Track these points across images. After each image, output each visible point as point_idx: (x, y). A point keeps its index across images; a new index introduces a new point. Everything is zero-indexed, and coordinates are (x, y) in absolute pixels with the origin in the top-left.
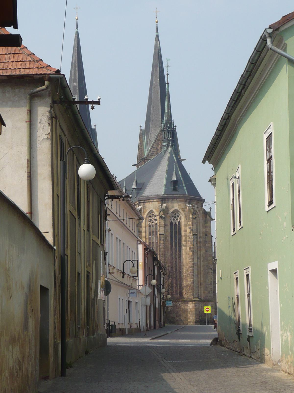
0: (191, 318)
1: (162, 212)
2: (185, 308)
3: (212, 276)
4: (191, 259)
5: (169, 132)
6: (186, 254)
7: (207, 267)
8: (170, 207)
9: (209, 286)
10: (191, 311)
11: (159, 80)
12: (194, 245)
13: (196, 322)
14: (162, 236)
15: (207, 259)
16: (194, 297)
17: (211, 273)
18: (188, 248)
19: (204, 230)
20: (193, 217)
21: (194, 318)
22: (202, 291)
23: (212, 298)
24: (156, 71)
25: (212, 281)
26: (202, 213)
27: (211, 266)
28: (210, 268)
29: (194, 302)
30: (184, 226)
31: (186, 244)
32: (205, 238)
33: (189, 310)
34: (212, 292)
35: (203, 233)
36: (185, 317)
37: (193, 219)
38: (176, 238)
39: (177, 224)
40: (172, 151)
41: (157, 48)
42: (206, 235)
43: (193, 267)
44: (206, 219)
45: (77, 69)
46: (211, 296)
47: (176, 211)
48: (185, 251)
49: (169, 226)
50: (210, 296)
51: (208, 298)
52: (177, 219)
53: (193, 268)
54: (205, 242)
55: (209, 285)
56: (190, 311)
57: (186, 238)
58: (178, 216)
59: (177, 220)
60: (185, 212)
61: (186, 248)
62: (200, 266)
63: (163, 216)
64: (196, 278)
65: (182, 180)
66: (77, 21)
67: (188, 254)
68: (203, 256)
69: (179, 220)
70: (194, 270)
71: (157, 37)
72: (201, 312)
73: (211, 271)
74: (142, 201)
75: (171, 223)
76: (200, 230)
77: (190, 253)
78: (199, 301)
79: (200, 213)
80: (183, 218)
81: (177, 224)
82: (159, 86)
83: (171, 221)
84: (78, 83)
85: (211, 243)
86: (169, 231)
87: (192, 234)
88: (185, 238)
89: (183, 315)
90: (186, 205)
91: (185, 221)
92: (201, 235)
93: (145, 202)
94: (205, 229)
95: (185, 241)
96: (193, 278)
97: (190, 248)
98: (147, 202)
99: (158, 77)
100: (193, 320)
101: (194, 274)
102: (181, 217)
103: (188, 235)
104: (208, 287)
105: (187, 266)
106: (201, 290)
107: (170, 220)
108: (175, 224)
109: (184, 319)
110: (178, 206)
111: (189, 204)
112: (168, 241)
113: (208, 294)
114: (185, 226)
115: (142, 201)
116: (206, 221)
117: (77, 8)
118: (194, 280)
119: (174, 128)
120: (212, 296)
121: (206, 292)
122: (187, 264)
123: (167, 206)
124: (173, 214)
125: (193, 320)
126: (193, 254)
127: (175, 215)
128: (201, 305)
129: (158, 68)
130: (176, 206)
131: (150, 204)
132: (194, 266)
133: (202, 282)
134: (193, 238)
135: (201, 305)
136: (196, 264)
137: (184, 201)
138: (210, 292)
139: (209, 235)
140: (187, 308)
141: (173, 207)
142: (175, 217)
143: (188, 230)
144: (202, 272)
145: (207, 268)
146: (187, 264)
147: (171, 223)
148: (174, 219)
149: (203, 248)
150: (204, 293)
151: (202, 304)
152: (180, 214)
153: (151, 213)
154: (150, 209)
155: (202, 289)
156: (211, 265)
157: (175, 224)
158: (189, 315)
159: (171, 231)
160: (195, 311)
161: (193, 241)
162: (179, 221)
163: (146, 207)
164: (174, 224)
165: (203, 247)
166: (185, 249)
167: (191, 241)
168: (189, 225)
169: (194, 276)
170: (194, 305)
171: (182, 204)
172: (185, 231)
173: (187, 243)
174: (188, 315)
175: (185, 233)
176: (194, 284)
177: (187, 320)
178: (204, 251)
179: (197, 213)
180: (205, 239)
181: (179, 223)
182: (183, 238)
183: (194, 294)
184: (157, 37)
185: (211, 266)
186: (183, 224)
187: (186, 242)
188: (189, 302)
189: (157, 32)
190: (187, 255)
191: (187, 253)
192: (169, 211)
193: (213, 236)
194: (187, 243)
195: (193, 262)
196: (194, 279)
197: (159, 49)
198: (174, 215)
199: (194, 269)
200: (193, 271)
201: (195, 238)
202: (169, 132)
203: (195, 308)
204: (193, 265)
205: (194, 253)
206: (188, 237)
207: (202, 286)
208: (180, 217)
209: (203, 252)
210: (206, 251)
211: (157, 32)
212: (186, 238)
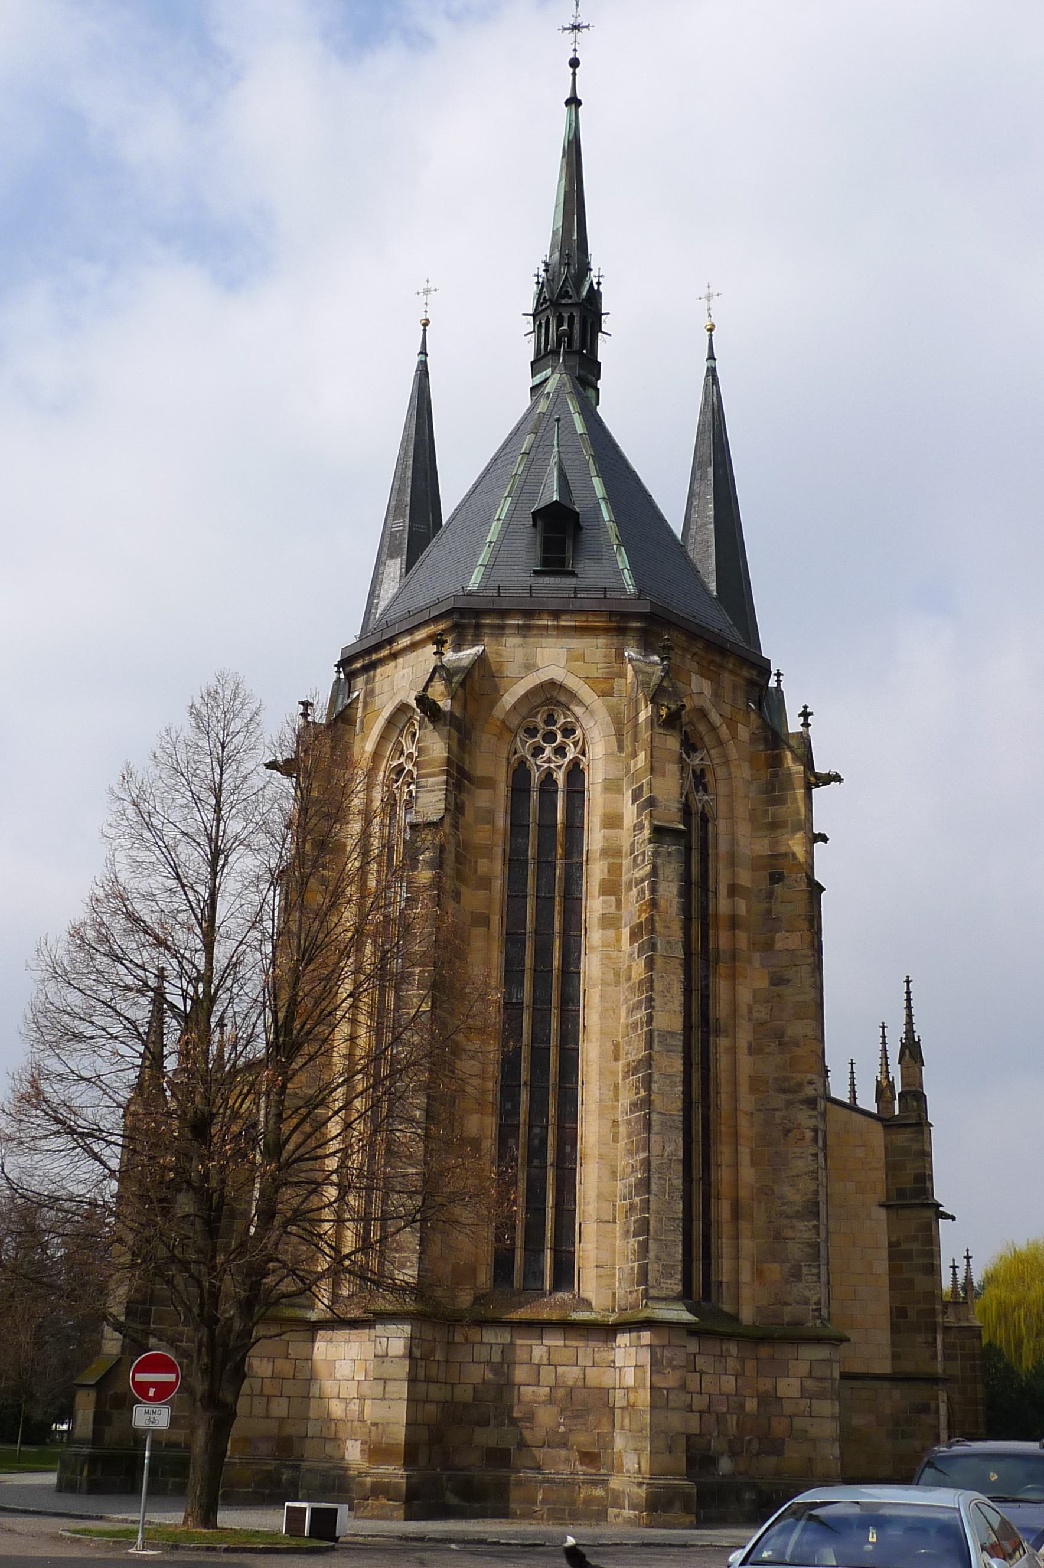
0: (630, 1462)
1: (441, 678)
2: (594, 1376)
3: (816, 1155)
4: (637, 1006)
5: (566, 316)
6: (611, 976)
7: (784, 1091)
8: (511, 669)
9: (793, 1228)
10: (630, 1407)
11: (712, 505)
12: (662, 903)
13: (658, 1504)
14: (428, 836)
15: (779, 1036)
16: (653, 1292)
17: (809, 1135)
18: (626, 932)
19: (762, 847)
20: (656, 714)
21: (645, 1467)
22: (746, 1266)
23: (820, 1317)
24: (703, 477)
25: (816, 1193)
26: (753, 739)
27: (810, 1083)
28: (801, 1096)
29: (646, 1337)
30: (606, 789)
31: (613, 909)
32: (770, 895)
33: (619, 1399)
34: (814, 1271)
35: (757, 863)
36: (589, 1458)
37: (657, 730)
38: (545, 864)
39: (560, 777)
40: (565, 385)
41: (710, 407)
42: (776, 878)
43: (649, 1061)
44: (775, 775)
45: (409, 474)
46: (815, 1299)
47: (551, 697)
48: (606, 958)
49: (503, 789)
50: (806, 1302)
51: (788, 1313)
52: (560, 751)
53: (650, 1067)
54: (771, 921)
55: (798, 1215)
56: (622, 1408)
57: (615, 870)
58: (568, 731)
59: (565, 755)
60: (613, 700)
61: (611, 933)
62: (735, 1083)
63: (445, 704)
64: (669, 1149)
65: (607, 518)
66: (425, 330)
67: (623, 979)
68: (755, 1015)
69: (571, 753)
70: (654, 1086)
71: (712, 372)
72: (732, 1420)
73: (810, 1117)
74: (358, 665)
75: (520, 774)
76: (733, 842)
77: (634, 964)
78: (689, 1330)
79: (734, 737)
80: (597, 739)
81: (560, 777)
82: (712, 526)
83: (522, 762)
84: (407, 520)
85: (805, 925)
86: (501, 820)
87: (647, 832)
88: (610, 865)
89: (574, 1438)
90: (619, 656)
91: (608, 755)
92: (745, 878)
93: (372, 666)
94: (766, 842)
95: (611, 888)
96: (647, 1146)
97: (634, 936)
98: (381, 662)
99: (711, 497)
100: (640, 1484)
101: (655, 1117)
102: (587, 735)
103: (626, 847)
104: (788, 1233)
105: (616, 1059)
106: (737, 1258)
107: (515, 753)
108: (549, 778)
109: (579, 1468)
110: (563, 662)
111: (647, 647)
112: (485, 883)
113: (788, 1282)
114: (612, 786)
115: (358, 665)
116: (773, 790)
117: (427, 292)
118: (655, 1163)
119: (595, 296)
120: (818, 1303)
121: (775, 1266)
122: (617, 1047)
123: (492, 658)
124: (535, 716)
125: (640, 1484)
126: (650, 964)
127: (551, 720)
128: (732, 1363)
129: (711, 469)
130: (547, 659)
131: (400, 666)
132: (656, 1056)
133: (743, 1193)
134: (656, 854)
135: (732, 1363)
136: (678, 1043)
137: (606, 631)
138: (805, 1270)
139: (794, 876)
140: (607, 1378)
141: (530, 667)
142: (550, 737)
143: (629, 813)
144: (744, 1122)
145: (784, 1096)
146: (617, 1047)
147: (520, 774)
148: (538, 751)
149: (757, 964)
150: (759, 1274)
151: (742, 1360)
152: (578, 710)
153: (401, 726)
154: (397, 701)
155: (747, 1245)
156: (810, 1076)
157: (542, 783)
158: (619, 1443)
159: (517, 826)
160: (653, 1407)
161: (654, 872)
162: (575, 763)
163: (377, 692)
164: (536, 777)
165: (757, 957)
166: (605, 945)
167: (642, 881)
168: (635, 777)
169: (655, 1129)
170: (645, 1357)
171: (595, 649)
172: (612, 821)
173: (619, 905)
174: (612, 1440)
175: (606, 838)
176: (654, 1187)
177: (604, 1483)
178: (764, 983)
179: (713, 729)
180: (764, 906)
181: (576, 773)
182: (596, 872)
183: (654, 1268)
184: (712, 372)
185: (810, 1083)
186: (595, 778)
187: (613, 898)
188: (623, 1331)
189: (711, 357)
190: (617, 984)
191: (617, 975)
192: (495, 694)
193: (824, 889)
194: (619, 905)
195: (650, 1019)
196: (656, 1149)
197: (716, 408)
198: (539, 720)
199: (656, 1077)
200: (649, 1089)
201: (669, 853)
202: (566, 316)
203: (652, 1387)
204: (650, 1045)
205: (659, 962)
206: (627, 862)
207: (744, 1226)
208: (578, 732)
209: (755, 991)
210: (778, 981)
211: (711, 357)
212: (615, 870)
